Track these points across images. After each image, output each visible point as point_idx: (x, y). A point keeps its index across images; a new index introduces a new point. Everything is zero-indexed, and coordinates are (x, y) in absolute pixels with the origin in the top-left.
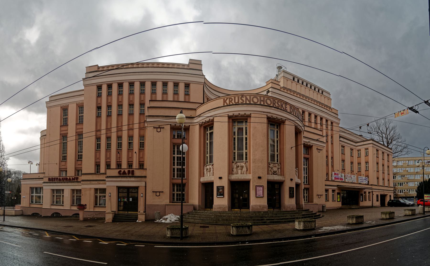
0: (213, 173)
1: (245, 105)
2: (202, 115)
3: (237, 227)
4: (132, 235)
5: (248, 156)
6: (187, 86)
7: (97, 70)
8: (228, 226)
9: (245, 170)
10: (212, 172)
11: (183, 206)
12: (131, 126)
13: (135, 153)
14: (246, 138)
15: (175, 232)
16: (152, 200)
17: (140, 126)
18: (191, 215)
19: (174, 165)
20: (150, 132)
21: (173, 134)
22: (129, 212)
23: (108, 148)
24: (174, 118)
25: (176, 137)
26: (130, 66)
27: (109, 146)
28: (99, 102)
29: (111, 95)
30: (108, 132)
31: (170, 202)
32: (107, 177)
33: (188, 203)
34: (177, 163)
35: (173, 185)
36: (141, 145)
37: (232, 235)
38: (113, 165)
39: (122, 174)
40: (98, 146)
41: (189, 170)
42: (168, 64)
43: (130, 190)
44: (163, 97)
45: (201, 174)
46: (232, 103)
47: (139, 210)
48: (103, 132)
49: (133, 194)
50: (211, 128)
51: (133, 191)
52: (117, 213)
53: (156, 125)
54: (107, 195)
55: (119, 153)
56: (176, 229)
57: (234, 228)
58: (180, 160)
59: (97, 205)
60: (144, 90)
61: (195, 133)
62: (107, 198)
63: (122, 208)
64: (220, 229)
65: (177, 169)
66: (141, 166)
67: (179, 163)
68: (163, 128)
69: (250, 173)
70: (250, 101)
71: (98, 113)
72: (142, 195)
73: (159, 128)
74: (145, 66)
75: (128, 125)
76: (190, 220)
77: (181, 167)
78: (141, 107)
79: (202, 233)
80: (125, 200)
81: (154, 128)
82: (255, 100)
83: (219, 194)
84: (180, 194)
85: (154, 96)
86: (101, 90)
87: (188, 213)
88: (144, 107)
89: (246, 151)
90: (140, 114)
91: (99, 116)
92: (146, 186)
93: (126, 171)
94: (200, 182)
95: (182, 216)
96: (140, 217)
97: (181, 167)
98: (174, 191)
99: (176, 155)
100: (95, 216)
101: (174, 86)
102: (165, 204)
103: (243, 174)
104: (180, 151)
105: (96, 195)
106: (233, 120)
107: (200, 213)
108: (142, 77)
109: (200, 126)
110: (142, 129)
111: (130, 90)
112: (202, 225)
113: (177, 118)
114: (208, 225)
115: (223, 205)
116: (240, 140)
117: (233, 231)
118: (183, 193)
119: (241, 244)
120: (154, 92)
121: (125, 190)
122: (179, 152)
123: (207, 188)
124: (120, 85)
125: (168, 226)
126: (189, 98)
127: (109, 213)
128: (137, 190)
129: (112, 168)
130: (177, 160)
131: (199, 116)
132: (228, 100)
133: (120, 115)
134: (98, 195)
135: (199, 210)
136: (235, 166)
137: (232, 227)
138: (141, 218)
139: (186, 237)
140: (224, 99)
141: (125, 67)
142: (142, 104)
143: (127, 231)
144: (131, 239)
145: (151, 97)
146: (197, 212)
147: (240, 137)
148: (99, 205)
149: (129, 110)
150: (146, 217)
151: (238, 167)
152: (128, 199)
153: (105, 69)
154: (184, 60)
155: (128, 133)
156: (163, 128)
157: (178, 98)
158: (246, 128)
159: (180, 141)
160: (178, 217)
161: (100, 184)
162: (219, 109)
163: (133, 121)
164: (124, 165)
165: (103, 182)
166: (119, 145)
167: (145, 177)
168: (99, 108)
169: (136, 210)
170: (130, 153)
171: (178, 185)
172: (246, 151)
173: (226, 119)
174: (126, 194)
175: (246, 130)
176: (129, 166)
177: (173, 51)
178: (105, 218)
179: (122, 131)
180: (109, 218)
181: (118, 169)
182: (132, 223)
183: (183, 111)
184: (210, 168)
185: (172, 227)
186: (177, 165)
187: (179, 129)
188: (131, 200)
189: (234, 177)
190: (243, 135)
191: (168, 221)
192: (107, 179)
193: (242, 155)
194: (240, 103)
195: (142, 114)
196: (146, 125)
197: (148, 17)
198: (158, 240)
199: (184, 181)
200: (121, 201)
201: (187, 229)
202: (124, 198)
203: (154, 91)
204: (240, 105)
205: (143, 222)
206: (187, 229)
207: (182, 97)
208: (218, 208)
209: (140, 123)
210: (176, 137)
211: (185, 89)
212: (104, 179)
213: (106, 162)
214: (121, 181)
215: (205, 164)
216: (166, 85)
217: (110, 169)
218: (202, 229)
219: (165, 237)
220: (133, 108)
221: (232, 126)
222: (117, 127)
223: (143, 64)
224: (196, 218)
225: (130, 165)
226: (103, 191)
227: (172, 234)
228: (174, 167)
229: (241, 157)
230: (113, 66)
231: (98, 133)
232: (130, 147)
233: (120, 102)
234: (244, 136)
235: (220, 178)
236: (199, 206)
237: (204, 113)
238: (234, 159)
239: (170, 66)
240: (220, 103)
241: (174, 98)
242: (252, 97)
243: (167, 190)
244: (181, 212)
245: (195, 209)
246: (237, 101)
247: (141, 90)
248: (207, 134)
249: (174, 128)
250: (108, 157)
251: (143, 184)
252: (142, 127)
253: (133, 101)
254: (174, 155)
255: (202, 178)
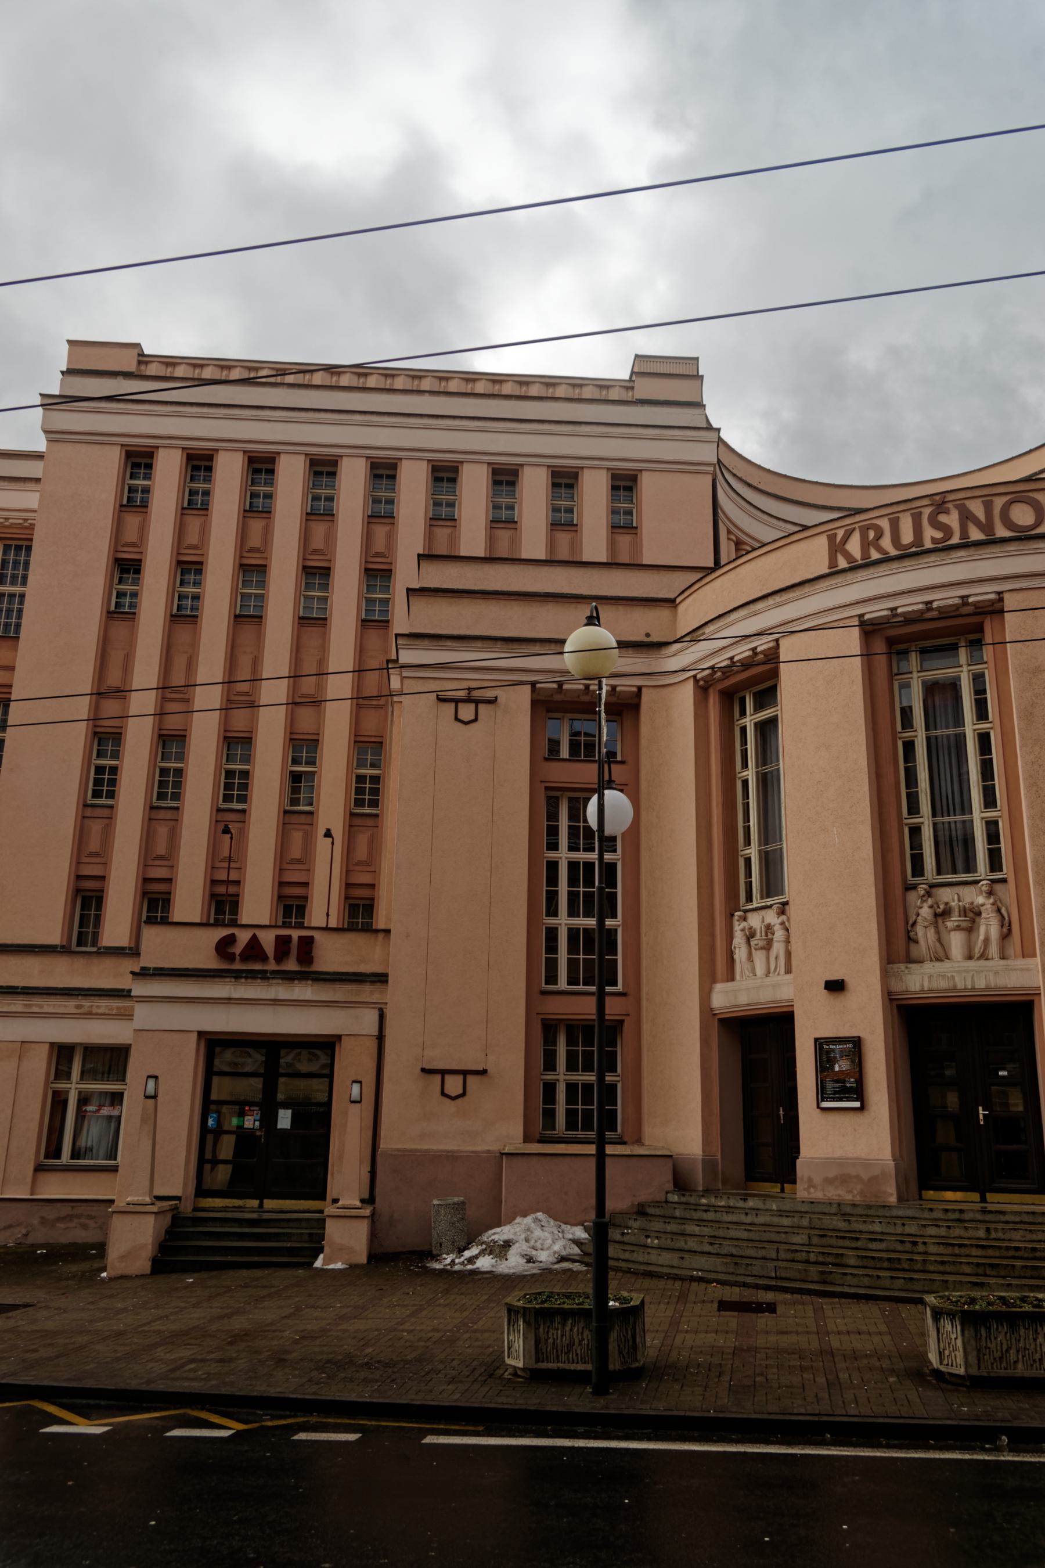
0: (788, 954)
1: (961, 553)
2: (708, 630)
3: (973, 1321)
4: (280, 1360)
5: (1004, 845)
6: (624, 484)
7: (132, 368)
8: (907, 1311)
9: (994, 932)
10: (778, 947)
11: (611, 1168)
12: (308, 685)
13: (328, 834)
14: (984, 740)
15: (557, 1334)
16: (415, 1123)
17: (358, 686)
18: (658, 1226)
19: (552, 911)
20: (415, 726)
21: (549, 734)
22: (269, 1204)
23: (161, 796)
24: (553, 648)
25: (565, 753)
26: (318, 379)
27: (167, 786)
28: (130, 535)
29: (205, 508)
30: (172, 707)
31: (527, 1139)
32: (144, 974)
33: (639, 1141)
34: (573, 897)
35: (549, 1028)
36: (359, 791)
37: (937, 1373)
38: (189, 900)
39: (241, 961)
40: (103, 783)
41: (644, 939)
42: (523, 381)
43: (286, 1058)
44: (491, 541)
45: (717, 964)
46: (880, 549)
47: (333, 1188)
48: (143, 703)
49: (302, 1084)
50: (767, 695)
51: (304, 1067)
52: (186, 1208)
53: (454, 684)
54: (134, 1087)
55: (226, 831)
56: (565, 1314)
57: (947, 1325)
58: (587, 1100)
59: (58, 1155)
60: (390, 502)
61: (675, 728)
62: (131, 1110)
63: (222, 1174)
64: (854, 1328)
65: (573, 934)
66: (360, 913)
67: (585, 904)
68: (493, 701)
69: (1027, 952)
70: (987, 527)
71: (120, 595)
72: (356, 1089)
73: (470, 702)
74: (399, 383)
75: (295, 676)
76: (653, 1257)
77: (592, 922)
78: (370, 588)
79: (736, 1351)
80: (251, 1122)
81: (441, 700)
82: (1022, 515)
83: (830, 1087)
84: (588, 1087)
85: (442, 533)
86: (148, 477)
87: (641, 1211)
88: (386, 589)
89: (991, 814)
90: (365, 623)
91: (120, 611)
92: (381, 1038)
93: (268, 939)
94: (706, 1010)
95: (600, 1232)
96: (333, 1230)
97: (592, 922)
98: (550, 1065)
99: (564, 855)
100: (41, 1235)
101: (555, 485)
102: (495, 1147)
103: (984, 956)
104: (588, 829)
105: (61, 1086)
106: (891, 642)
107: (716, 1209)
108: (385, 438)
109: (703, 688)
110: (371, 702)
111: (316, 498)
112: (733, 1294)
113: (567, 647)
114: (770, 1296)
115: (866, 1164)
116: (947, 753)
117: (947, 1348)
118: (609, 1078)
119: (1013, 1449)
120: (442, 515)
121: (254, 1061)
122: (582, 836)
123: (756, 1048)
124: (261, 466)
125: (515, 1299)
126: (636, 547)
127: (133, 1211)
128: (324, 1059)
129: (177, 916)
130: (573, 881)
131: (694, 635)
132: (856, 538)
133: (247, 618)
134: (74, 1087)
135: (707, 1192)
136: (926, 911)
137: (937, 1314)
138: (346, 1242)
139: (633, 1375)
140: (832, 538)
141: (290, 379)
142: (377, 574)
143: (246, 1335)
144: (273, 1392)
145: (430, 538)
146: (696, 1207)
147: (941, 732)
148: (75, 1154)
149: (302, 597)
150: (373, 1236)
151: (946, 913)
152: (269, 1119)
153: (180, 371)
154: (607, 361)
155: (291, 721)
156: (493, 701)
157: (575, 545)
158: (978, 679)
159: (586, 773)
160: (580, 1233)
161: (89, 1015)
162: (806, 589)
163: (322, 661)
164: (257, 906)
165: (115, 1004)
166: (235, 786)
167: (381, 979)
168: (127, 567)
169: (315, 1185)
170: (297, 837)
171: (578, 1031)
172: (991, 814)
173: (852, 640)
174: (257, 1083)
175: (980, 691)
176: (287, 911)
177: (547, 321)
178: (101, 1248)
179: (253, 706)
180: (132, 1242)
181: (218, 924)
182: (281, 1278)
183: (605, 613)
184: (769, 928)
185: (539, 1306)
186: (572, 912)
187: (583, 705)
188: (284, 1120)
189: (923, 980)
190: (959, 721)
191: (513, 1263)
192: (139, 989)
193: (968, 841)
194: (928, 545)
195: (373, 621)
196: (395, 683)
197: (421, 164)
198: (447, 1394)
199: (613, 1008)
200: (219, 1132)
201: (632, 1314)
202: (241, 1107)
203: (444, 511)
204: (933, 558)
205: (353, 1267)
206: (632, 1314)
207: (594, 542)
208: (829, 1181)
209: (359, 671)
210: (565, 753)
211: (614, 498)
212: (124, 982)
213: (146, 880)
214: (229, 1001)
215: (735, 903)
216: (512, 484)
217: (165, 922)
218: (732, 1319)
219: (492, 1369)
220: (325, 587)
221: (891, 676)
222: (229, 682)
223: (390, 374)
224: (692, 1244)
225: (292, 905)
226: (111, 1060)
227: (538, 1350)
228: (551, 921)
229: (956, 853)
230: (225, 364)
231: (111, 707)
232: (295, 802)
233: (252, 550)
234: (970, 728)
235: (835, 987)
236: (709, 1164)
237: (719, 620)
238: (918, 868)
239: (534, 391)
240: (812, 558)
241: (551, 544)
242: (999, 503)
243: (510, 1059)
244: (593, 1201)
245: (681, 1182)
246: (907, 536)
247: (376, 501)
248: (744, 730)
249: (550, 704)
250: (161, 849)
251: (367, 1022)
252: (371, 690)
253: (328, 550)
254: (552, 855)
255: (719, 987)
